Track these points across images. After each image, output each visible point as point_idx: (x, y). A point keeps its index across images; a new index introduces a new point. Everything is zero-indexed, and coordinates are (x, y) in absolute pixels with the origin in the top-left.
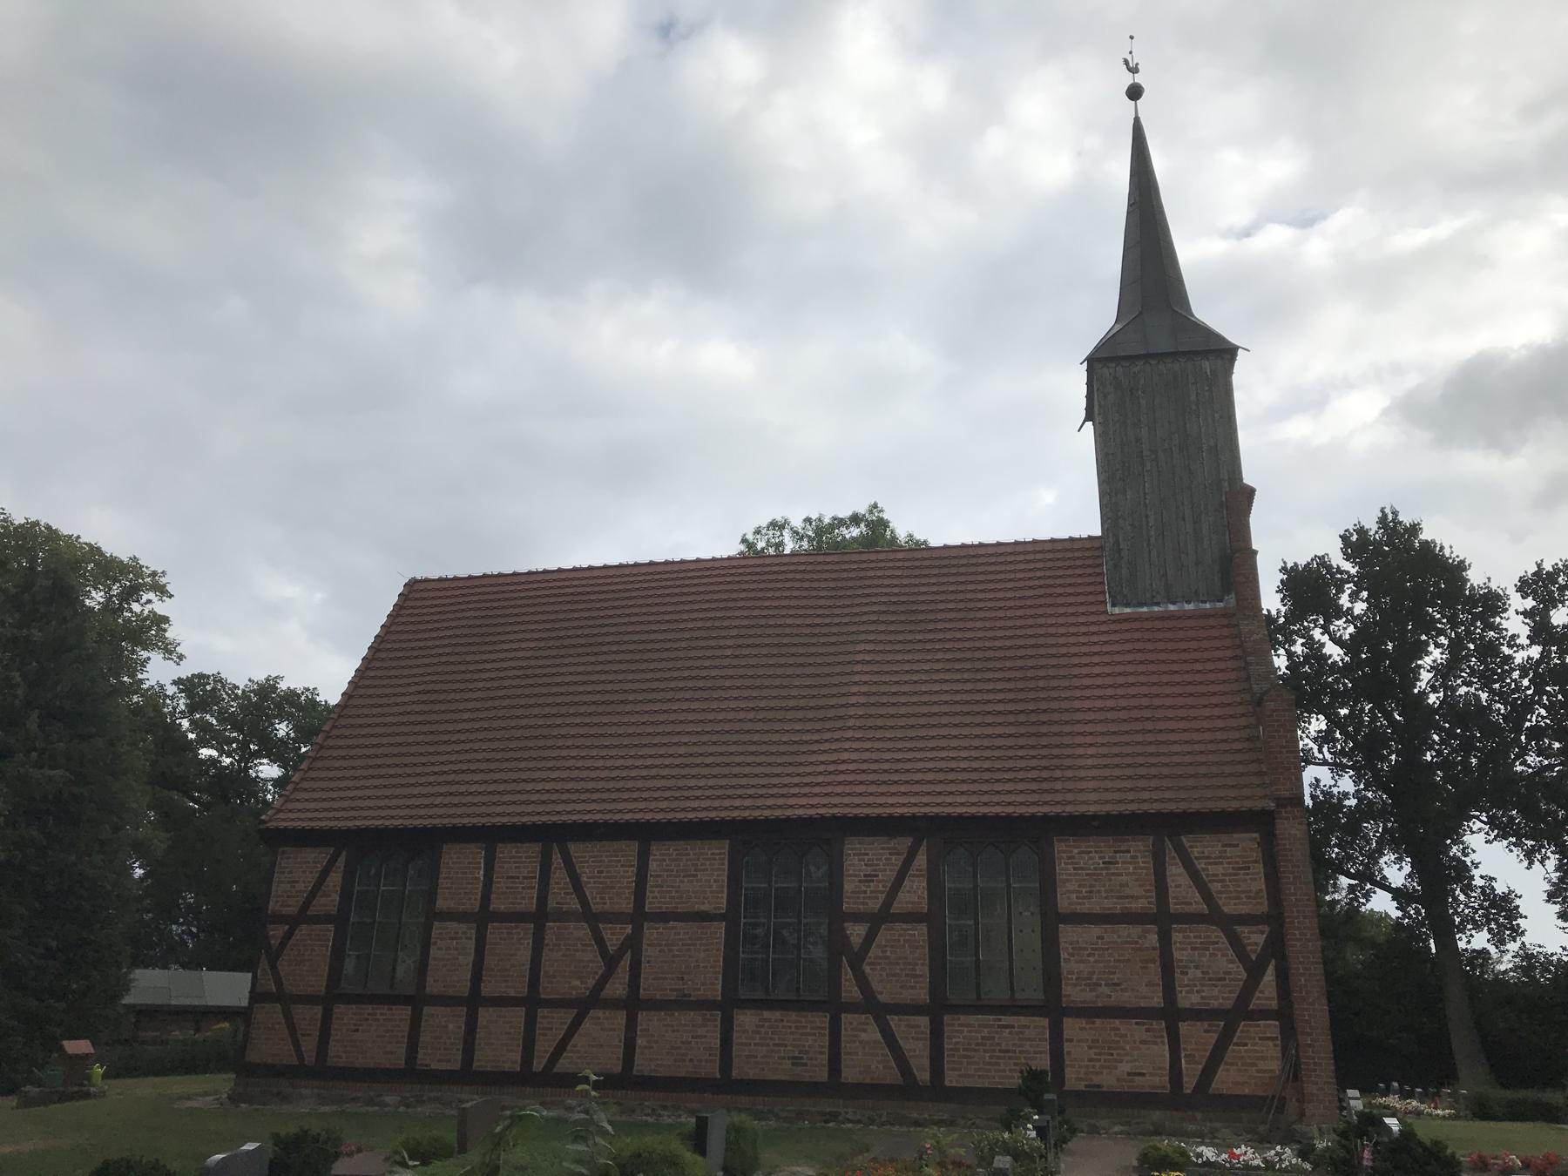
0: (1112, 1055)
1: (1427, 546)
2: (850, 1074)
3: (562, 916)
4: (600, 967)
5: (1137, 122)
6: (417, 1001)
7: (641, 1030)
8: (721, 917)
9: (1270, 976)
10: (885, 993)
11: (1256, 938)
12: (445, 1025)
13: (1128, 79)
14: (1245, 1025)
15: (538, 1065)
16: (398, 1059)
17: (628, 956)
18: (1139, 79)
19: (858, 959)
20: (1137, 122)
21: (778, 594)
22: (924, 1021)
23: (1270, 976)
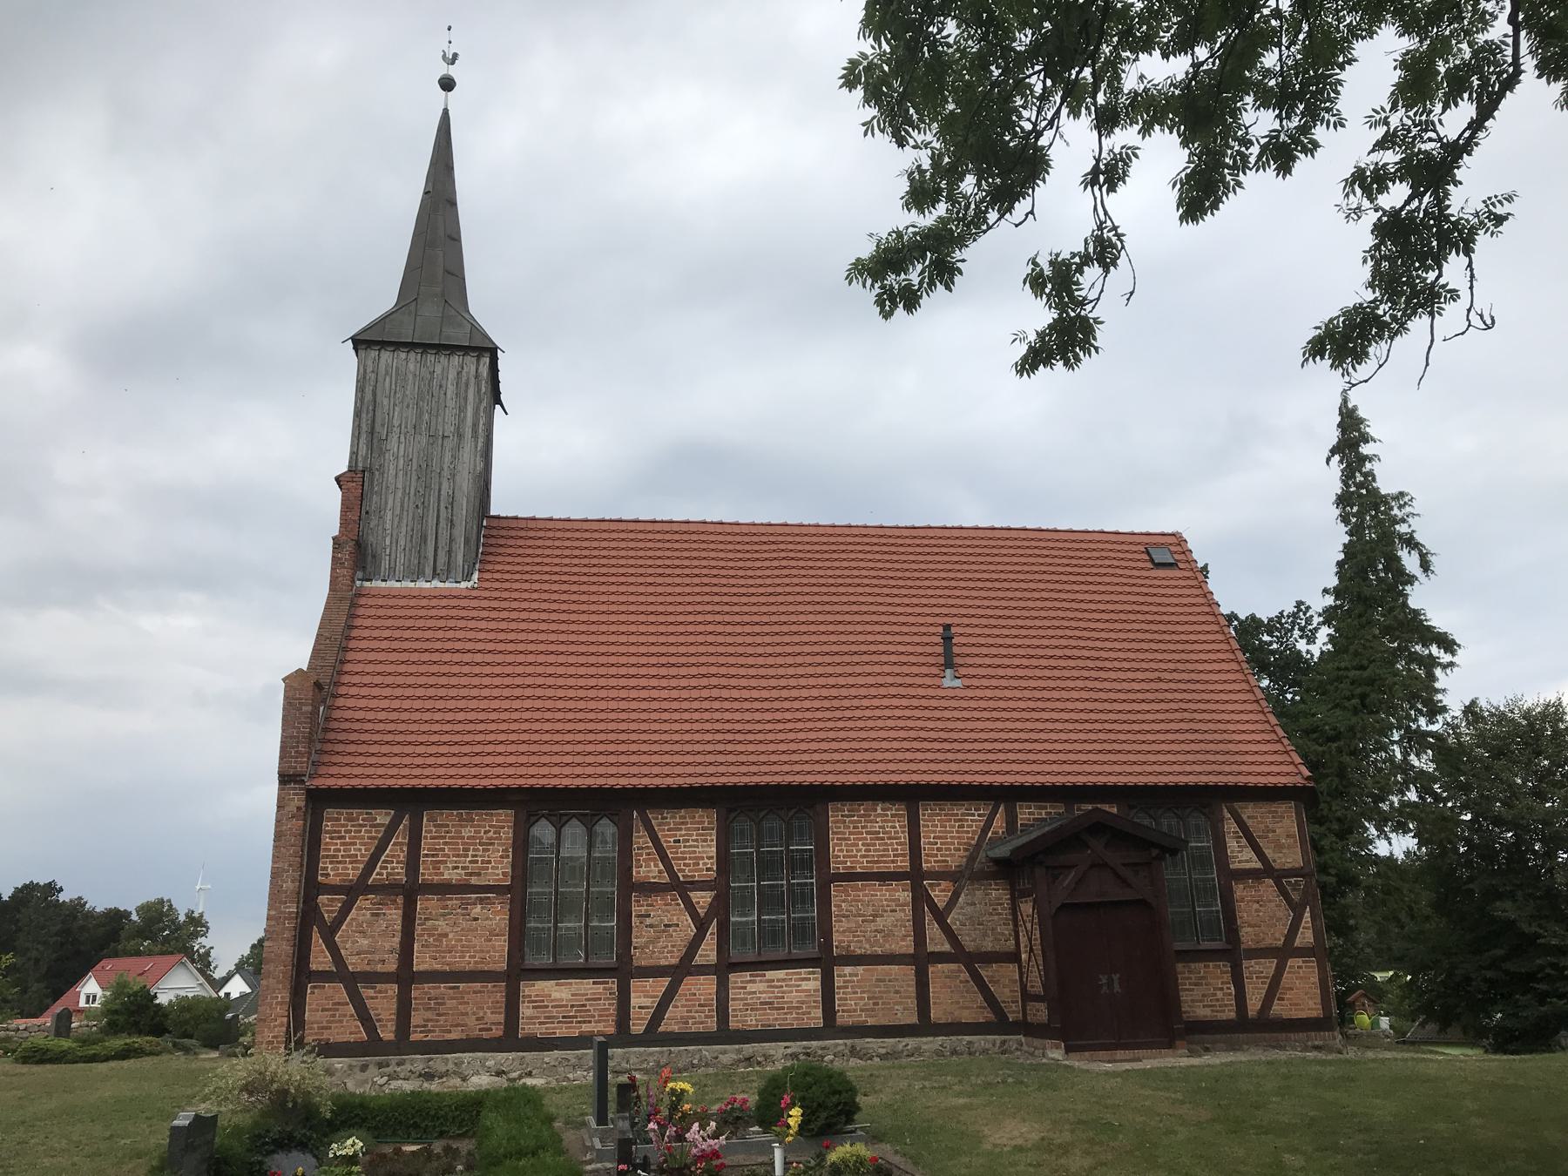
0: (843, 993)
1: (1340, 574)
2: (842, 1019)
3: (650, 889)
4: (692, 930)
5: (446, 113)
6: (623, 972)
7: (310, 1010)
8: (508, 889)
9: (713, 928)
10: (354, 963)
11: (702, 899)
12: (643, 996)
13: (443, 69)
14: (312, 987)
15: (638, 1027)
16: (712, 1025)
17: (928, 917)
18: (453, 71)
19: (329, 933)
20: (446, 113)
21: (1064, 578)
22: (393, 989)
23: (713, 928)
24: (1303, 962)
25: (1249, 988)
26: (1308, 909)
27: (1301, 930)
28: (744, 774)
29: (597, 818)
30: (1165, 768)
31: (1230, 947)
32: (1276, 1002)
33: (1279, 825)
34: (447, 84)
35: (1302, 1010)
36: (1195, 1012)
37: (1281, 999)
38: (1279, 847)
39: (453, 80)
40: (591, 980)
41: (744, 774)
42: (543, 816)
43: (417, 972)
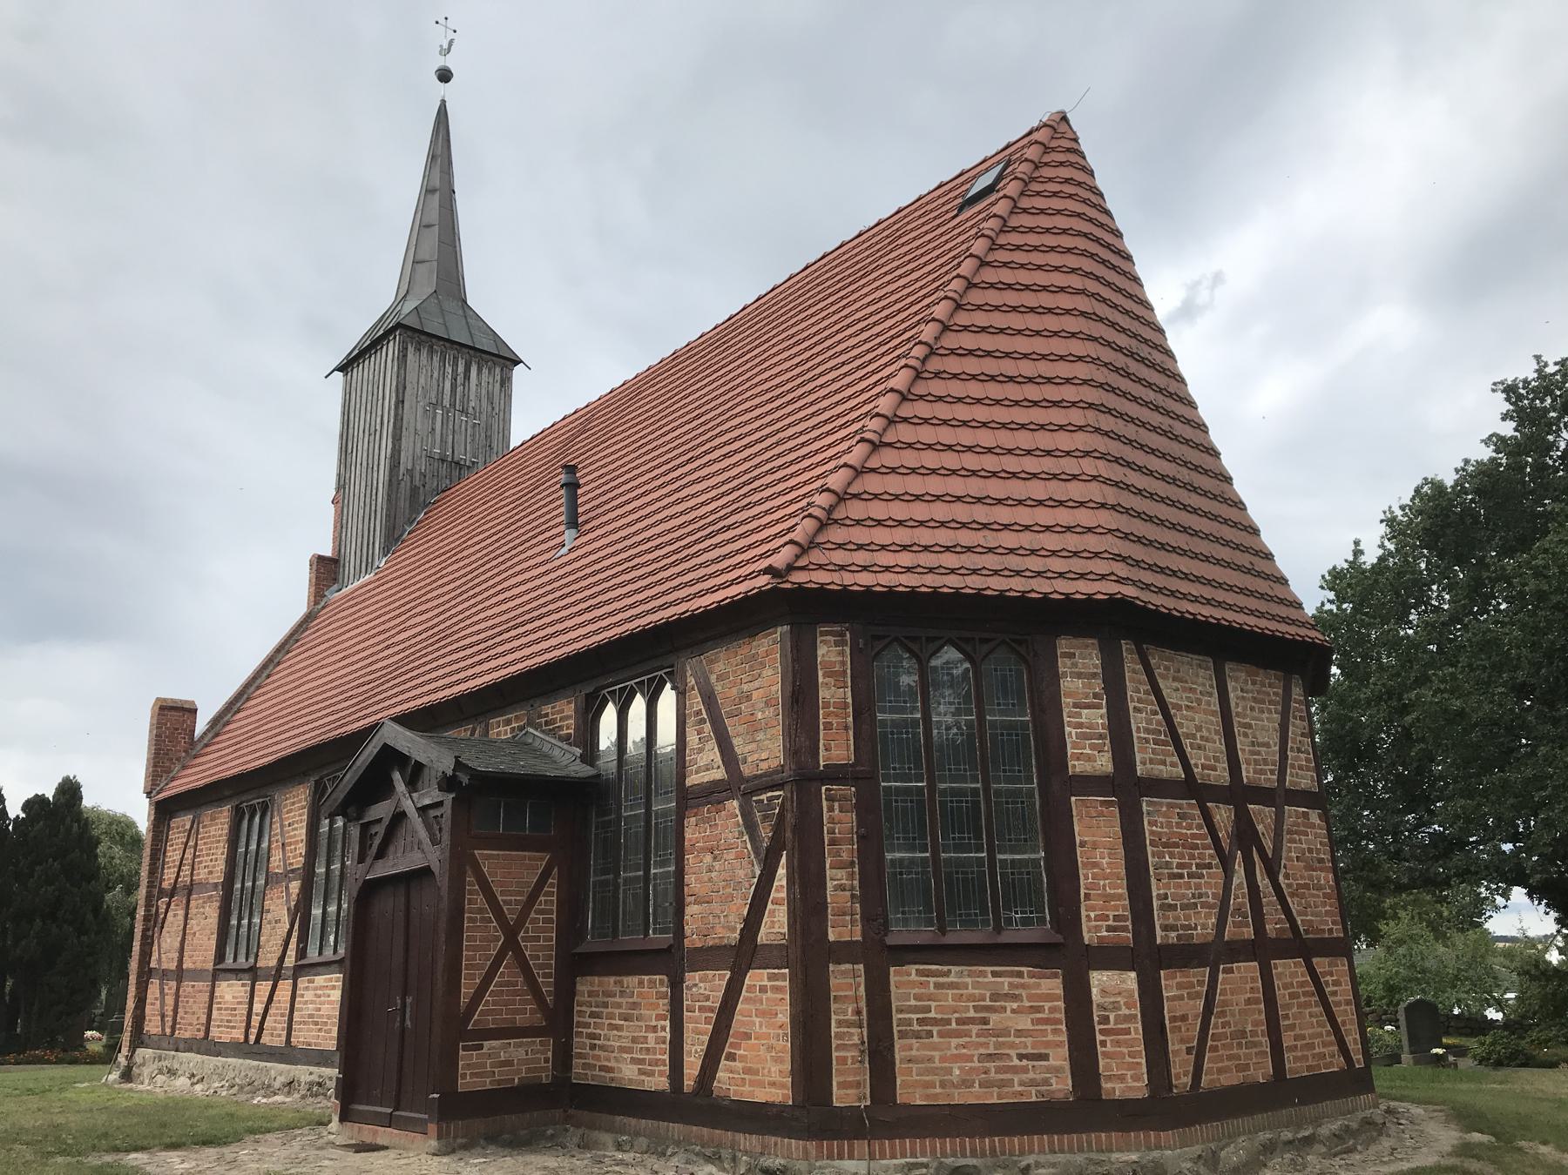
5: (443, 102)
18: (450, 62)
20: (443, 102)
24: (770, 979)
25: (688, 1027)
26: (783, 860)
27: (770, 906)
28: (865, 568)
29: (937, 644)
30: (536, 648)
31: (1059, 938)
32: (723, 1062)
33: (756, 684)
34: (445, 76)
35: (761, 1084)
36: (620, 1071)
37: (731, 1057)
38: (754, 727)
39: (450, 72)
40: (989, 969)
41: (865, 568)
42: (896, 639)
43: (764, 945)
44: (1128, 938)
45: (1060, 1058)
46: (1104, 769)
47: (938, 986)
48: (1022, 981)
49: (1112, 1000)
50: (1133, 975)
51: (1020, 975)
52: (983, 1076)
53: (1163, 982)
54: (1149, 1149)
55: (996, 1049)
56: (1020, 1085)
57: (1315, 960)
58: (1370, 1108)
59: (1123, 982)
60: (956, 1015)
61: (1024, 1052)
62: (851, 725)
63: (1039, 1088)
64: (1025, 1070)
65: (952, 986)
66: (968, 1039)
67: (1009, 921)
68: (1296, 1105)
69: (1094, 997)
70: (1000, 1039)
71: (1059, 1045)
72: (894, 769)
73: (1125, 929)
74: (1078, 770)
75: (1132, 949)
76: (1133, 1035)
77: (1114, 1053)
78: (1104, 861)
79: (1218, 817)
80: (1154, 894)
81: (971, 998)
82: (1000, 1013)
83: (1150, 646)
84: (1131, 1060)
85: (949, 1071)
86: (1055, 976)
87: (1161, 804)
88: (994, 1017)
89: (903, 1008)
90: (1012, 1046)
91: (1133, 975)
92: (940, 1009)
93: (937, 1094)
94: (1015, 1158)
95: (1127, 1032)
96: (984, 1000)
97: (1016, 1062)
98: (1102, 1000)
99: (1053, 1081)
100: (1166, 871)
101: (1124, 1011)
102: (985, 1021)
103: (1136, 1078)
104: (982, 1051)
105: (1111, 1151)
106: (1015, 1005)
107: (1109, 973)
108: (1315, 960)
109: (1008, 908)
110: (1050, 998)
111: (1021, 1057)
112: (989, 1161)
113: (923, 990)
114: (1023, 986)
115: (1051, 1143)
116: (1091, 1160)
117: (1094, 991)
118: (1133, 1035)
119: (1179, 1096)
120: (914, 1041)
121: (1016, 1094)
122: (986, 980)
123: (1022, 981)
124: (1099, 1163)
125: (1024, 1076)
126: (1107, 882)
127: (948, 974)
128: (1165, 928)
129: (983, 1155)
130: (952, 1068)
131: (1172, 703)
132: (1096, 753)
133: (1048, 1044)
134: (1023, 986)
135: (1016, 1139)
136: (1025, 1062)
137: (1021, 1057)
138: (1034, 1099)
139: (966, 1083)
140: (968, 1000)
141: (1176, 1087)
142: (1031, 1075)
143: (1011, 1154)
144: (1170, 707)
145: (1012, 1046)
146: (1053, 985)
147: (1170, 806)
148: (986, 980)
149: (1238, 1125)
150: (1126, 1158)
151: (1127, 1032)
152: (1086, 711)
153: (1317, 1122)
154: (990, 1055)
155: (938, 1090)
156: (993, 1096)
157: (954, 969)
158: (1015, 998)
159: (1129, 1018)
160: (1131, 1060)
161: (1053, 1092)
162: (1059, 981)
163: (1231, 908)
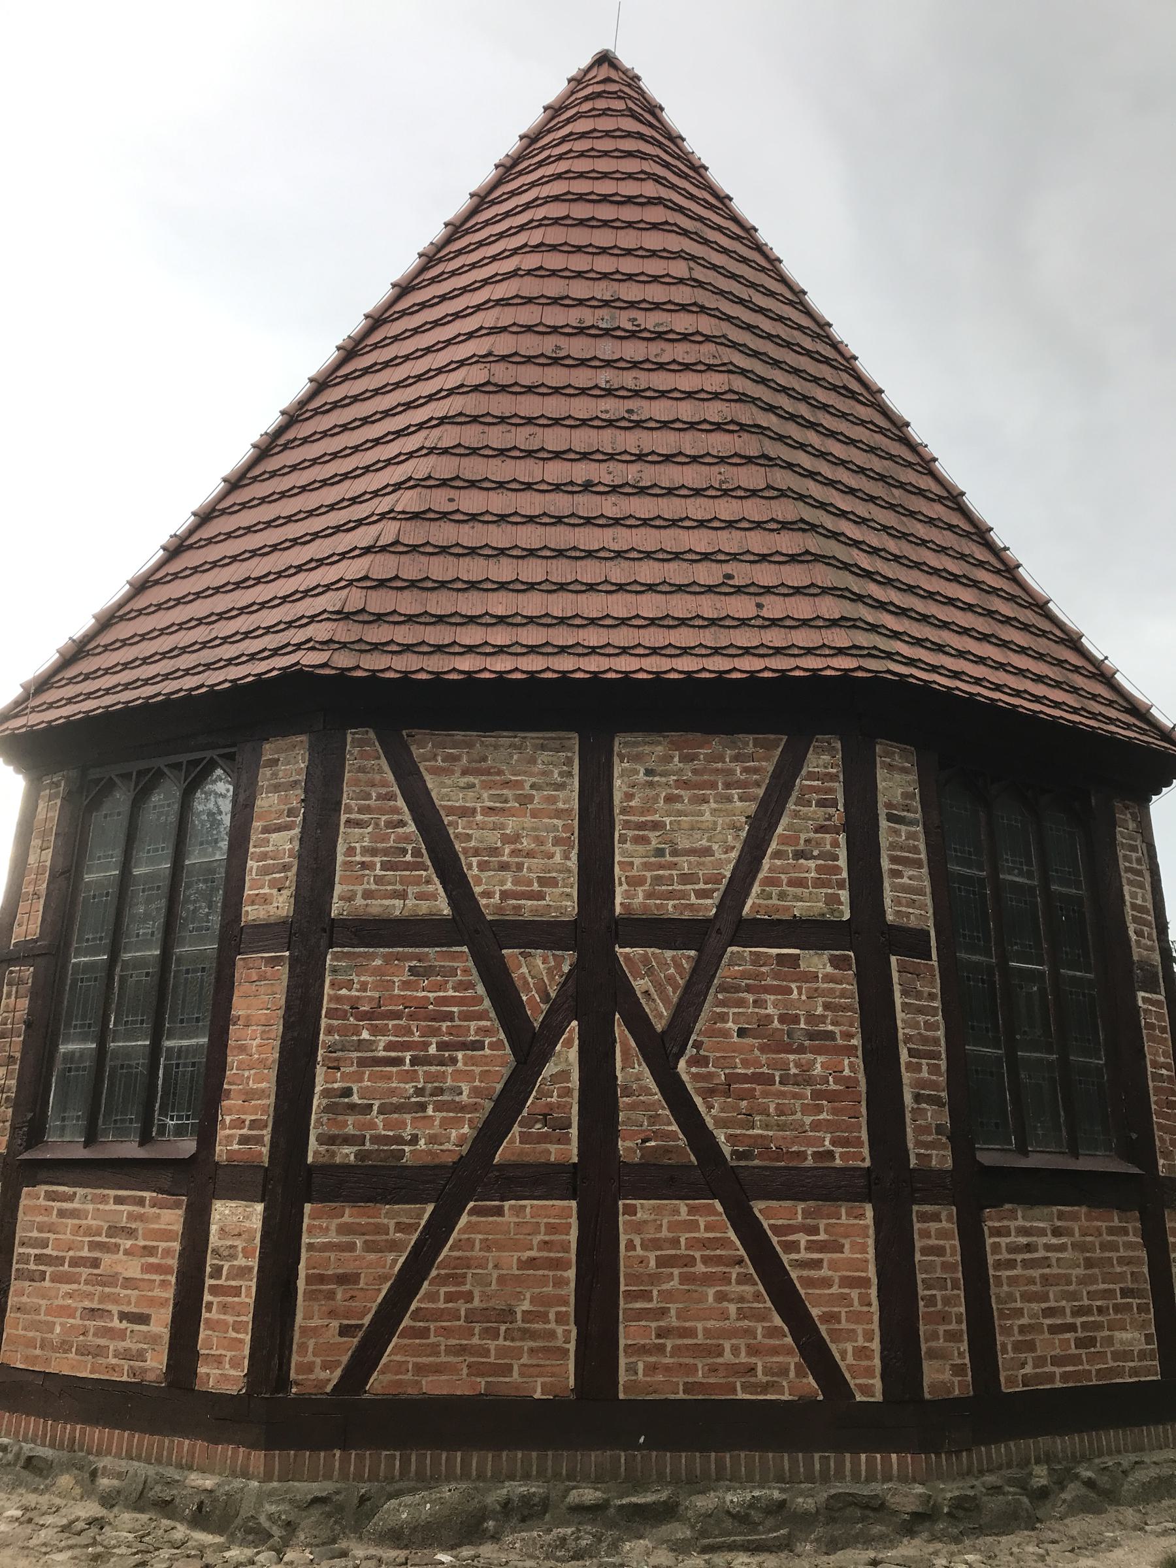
44: (261, 1153)
45: (161, 1324)
46: (279, 912)
47: (62, 1213)
48: (142, 1210)
49: (229, 1243)
50: (259, 1207)
51: (141, 1202)
52: (81, 1338)
53: (306, 1221)
54: (234, 1474)
55: (100, 1302)
56: (115, 1356)
57: (758, 1206)
58: (890, 1480)
59: (247, 1218)
60: (71, 1253)
61: (126, 1309)
62: (44, 893)
63: (132, 1363)
64: (121, 1335)
65: (74, 1214)
66: (75, 1286)
67: (162, 1128)
68: (639, 1447)
69: (211, 1237)
70: (107, 1290)
71: (163, 1303)
72: (88, 940)
73: (258, 1140)
74: (250, 918)
75: (266, 1169)
76: (243, 1298)
77: (218, 1321)
78: (255, 1043)
79: (524, 970)
80: (318, 1089)
81: (89, 1232)
82: (113, 1253)
83: (414, 732)
84: (234, 1335)
85: (51, 1327)
86: (177, 1206)
87: (373, 956)
88: (107, 1259)
89: (26, 1240)
90: (116, 1300)
91: (259, 1207)
92: (58, 1245)
93: (37, 1357)
94: (91, 1458)
95: (237, 1291)
96: (100, 1235)
97: (116, 1323)
98: (220, 1243)
99: (149, 1355)
100: (356, 1054)
101: (241, 1261)
102: (95, 1263)
103: (235, 1364)
104: (87, 1304)
105: (190, 1468)
106: (129, 1243)
107: (233, 1204)
108: (758, 1206)
109: (164, 1112)
110: (166, 1235)
111: (123, 1316)
112: (64, 1455)
113: (46, 1219)
114: (141, 1218)
115: (465, 1464)
116: (162, 1476)
117: (214, 1228)
118: (243, 1298)
119: (304, 1401)
120: (27, 1283)
121: (108, 1367)
122: (107, 1208)
123: (142, 1210)
124: (170, 1483)
125: (122, 1345)
126: (252, 1072)
127: (71, 1198)
128: (329, 1140)
129: (61, 1447)
130: (54, 1323)
131: (444, 807)
132: (275, 891)
133: (152, 1301)
134: (141, 1218)
135: (490, 1455)
136: (125, 1324)
137: (123, 1316)
138: (125, 1378)
139: (65, 1347)
140: (85, 1235)
141: (297, 1384)
142: (127, 1344)
143: (89, 1453)
144: (442, 813)
145: (116, 1300)
146: (172, 1219)
147: (387, 959)
148: (107, 1208)
149: (101, 1439)
150: (200, 1482)
151: (237, 1291)
152: (274, 835)
153: (698, 1483)
154: (93, 1310)
155: (38, 1352)
156: (86, 1367)
157: (80, 1191)
158: (131, 1233)
159: (243, 1272)
160: (234, 1335)
161: (145, 1371)
162: (180, 1212)
163: (525, 1113)
